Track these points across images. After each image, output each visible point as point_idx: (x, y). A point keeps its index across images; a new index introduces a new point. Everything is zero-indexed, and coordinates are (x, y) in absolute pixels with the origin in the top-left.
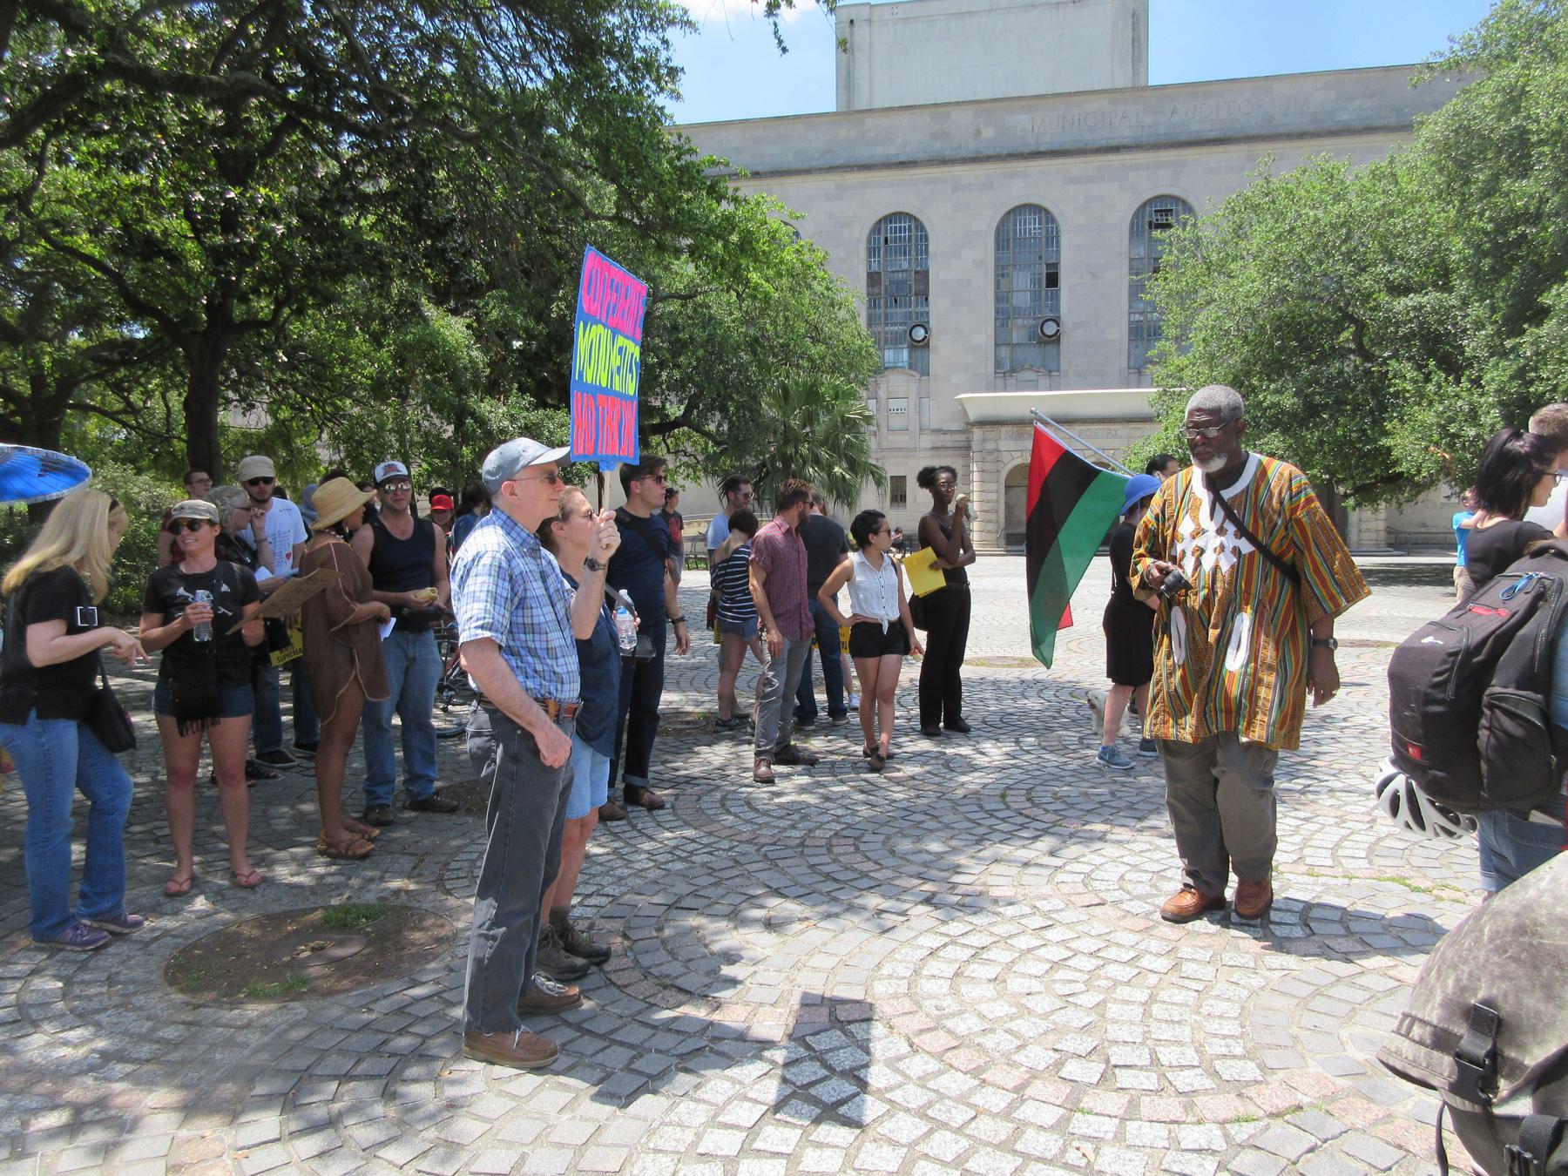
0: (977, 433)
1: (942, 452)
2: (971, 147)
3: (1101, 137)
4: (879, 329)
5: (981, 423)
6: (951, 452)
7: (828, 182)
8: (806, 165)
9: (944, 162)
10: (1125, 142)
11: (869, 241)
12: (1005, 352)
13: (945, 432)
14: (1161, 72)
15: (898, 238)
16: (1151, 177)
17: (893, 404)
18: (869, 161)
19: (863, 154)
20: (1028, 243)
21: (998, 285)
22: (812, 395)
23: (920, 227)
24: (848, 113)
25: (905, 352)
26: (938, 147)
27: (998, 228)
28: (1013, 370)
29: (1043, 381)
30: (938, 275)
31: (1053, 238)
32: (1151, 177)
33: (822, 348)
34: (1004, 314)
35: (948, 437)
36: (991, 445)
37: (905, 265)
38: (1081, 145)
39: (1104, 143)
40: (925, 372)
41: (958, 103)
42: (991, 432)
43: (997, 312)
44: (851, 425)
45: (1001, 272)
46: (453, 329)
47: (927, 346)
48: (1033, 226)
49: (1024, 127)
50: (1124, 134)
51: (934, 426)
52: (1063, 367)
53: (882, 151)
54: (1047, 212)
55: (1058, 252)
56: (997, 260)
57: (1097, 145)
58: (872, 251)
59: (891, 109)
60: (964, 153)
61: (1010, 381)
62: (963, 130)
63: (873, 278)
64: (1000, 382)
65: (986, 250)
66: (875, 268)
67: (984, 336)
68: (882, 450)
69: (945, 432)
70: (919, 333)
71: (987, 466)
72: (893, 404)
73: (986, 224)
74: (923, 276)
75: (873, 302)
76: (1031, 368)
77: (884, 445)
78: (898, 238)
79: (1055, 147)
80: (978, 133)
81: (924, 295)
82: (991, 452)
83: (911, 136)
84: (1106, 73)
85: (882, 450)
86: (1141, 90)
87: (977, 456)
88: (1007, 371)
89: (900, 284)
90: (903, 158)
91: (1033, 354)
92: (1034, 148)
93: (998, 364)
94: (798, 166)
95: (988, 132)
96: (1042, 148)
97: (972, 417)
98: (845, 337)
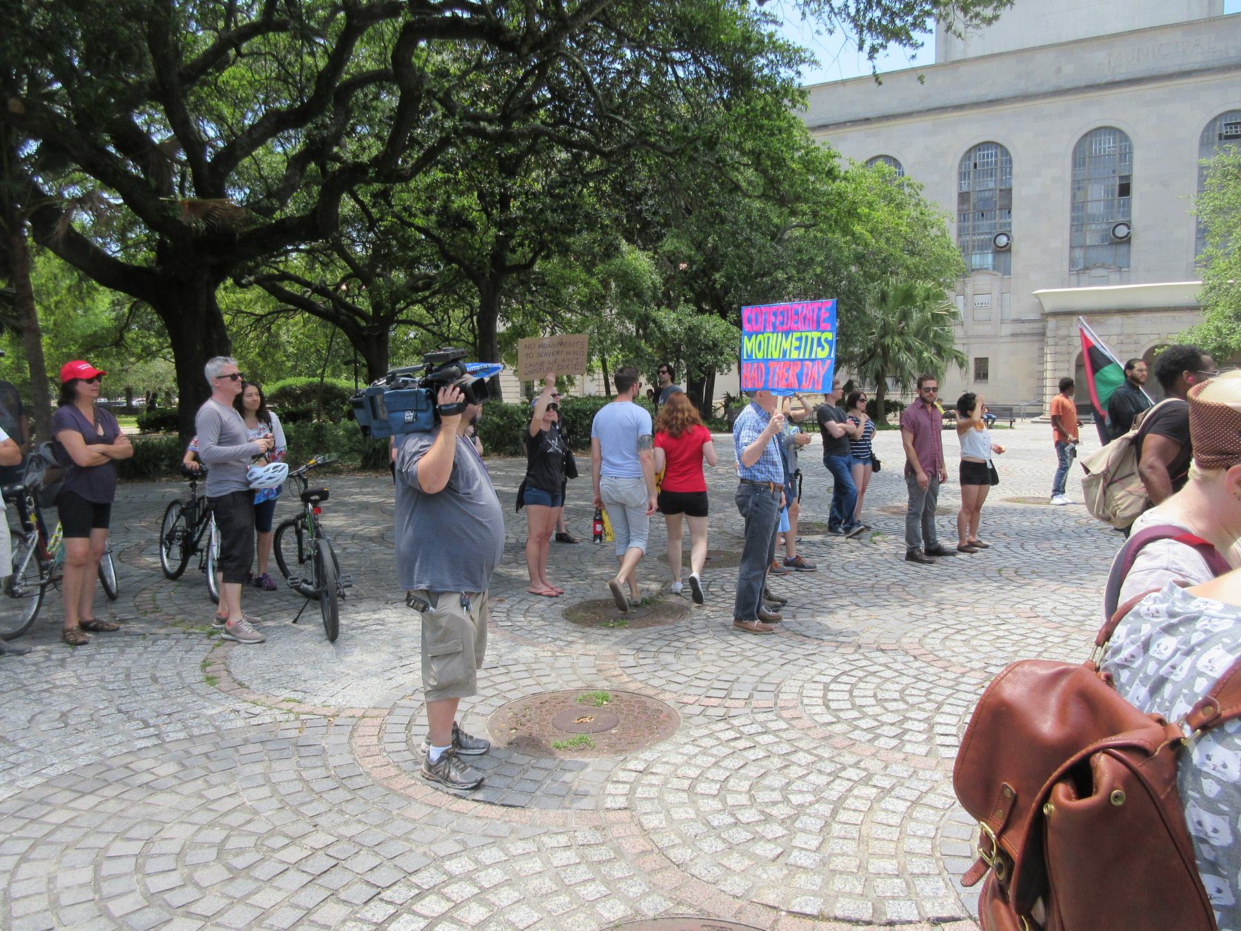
2: (1052, 83)
5: (1055, 314)
7: (926, 123)
8: (908, 109)
10: (1197, 66)
11: (960, 166)
12: (1079, 253)
13: (1023, 322)
15: (987, 170)
16: (974, 129)
18: (956, 103)
19: (956, 97)
21: (1074, 197)
22: (908, 297)
23: (1005, 152)
25: (990, 257)
26: (1022, 86)
28: (1086, 268)
29: (1114, 276)
30: (1021, 191)
31: (1126, 154)
32: (974, 129)
34: (1079, 220)
35: (1026, 325)
36: (1063, 332)
37: (991, 185)
38: (1155, 73)
39: (1176, 69)
40: (1007, 272)
41: (1041, 48)
42: (1064, 321)
43: (1073, 219)
44: (937, 318)
45: (1078, 186)
46: (638, 260)
48: (1107, 145)
49: (1102, 64)
50: (1196, 59)
52: (1133, 263)
53: (972, 94)
55: (1131, 166)
56: (1074, 175)
57: (1170, 70)
58: (963, 175)
59: (983, 57)
60: (1046, 88)
61: (1083, 278)
62: (1045, 72)
63: (963, 197)
64: (1074, 278)
66: (965, 189)
67: (1060, 240)
69: (1023, 322)
70: (1003, 240)
71: (1059, 349)
75: (963, 216)
76: (1103, 266)
77: (970, 333)
78: (987, 170)
80: (1059, 70)
82: (1064, 338)
83: (998, 81)
85: (968, 338)
87: (1050, 341)
88: (1081, 268)
89: (986, 201)
91: (1106, 254)
93: (1072, 263)
95: (1068, 69)
97: (1047, 310)
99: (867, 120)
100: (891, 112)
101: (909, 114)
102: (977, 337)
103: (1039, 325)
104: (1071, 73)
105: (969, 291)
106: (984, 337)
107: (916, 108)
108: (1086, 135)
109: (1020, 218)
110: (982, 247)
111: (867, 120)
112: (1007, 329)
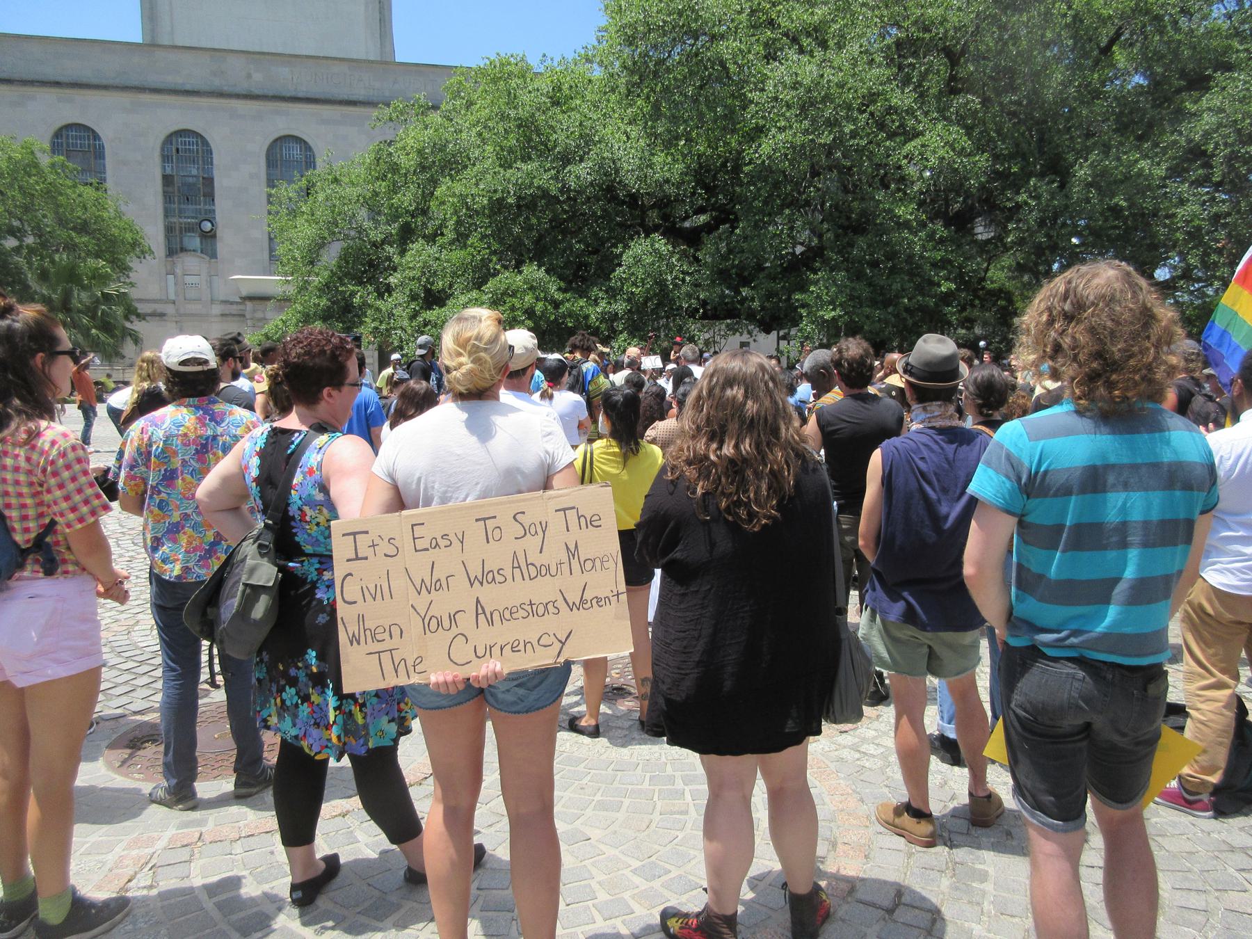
0: (249, 304)
1: (229, 318)
2: (243, 87)
3: (344, 93)
4: (174, 220)
5: (251, 298)
6: (236, 319)
7: (125, 99)
9: (221, 95)
10: (361, 99)
11: (163, 149)
13: (232, 303)
14: (405, 52)
17: (189, 279)
19: (153, 79)
20: (288, 157)
22: (72, 276)
23: (205, 142)
24: (151, 46)
25: (198, 240)
26: (217, 83)
27: (268, 150)
33: (85, 239)
35: (235, 307)
36: (259, 315)
37: (194, 172)
40: (213, 255)
41: (232, 51)
44: (107, 297)
47: (214, 236)
48: (296, 152)
51: (222, 298)
54: (305, 142)
56: (268, 175)
58: (166, 158)
60: (238, 90)
62: (237, 75)
63: (167, 180)
65: (259, 166)
66: (168, 171)
68: (181, 315)
69: (232, 303)
70: (207, 226)
72: (189, 279)
73: (259, 147)
74: (209, 181)
75: (168, 197)
77: (182, 311)
79: (309, 95)
80: (249, 76)
81: (210, 196)
83: (195, 73)
84: (361, 46)
85: (181, 315)
86: (386, 64)
90: (188, 87)
92: (293, 94)
94: (95, 81)
95: (258, 77)
96: (300, 95)
97: (244, 294)
98: (115, 231)
99: (57, 84)
100: (85, 81)
101: (105, 87)
102: (186, 315)
103: (242, 307)
104: (258, 80)
105: (178, 271)
106: (193, 315)
107: (111, 82)
108: (276, 141)
109: (223, 206)
110: (189, 229)
111: (57, 84)
112: (217, 309)
